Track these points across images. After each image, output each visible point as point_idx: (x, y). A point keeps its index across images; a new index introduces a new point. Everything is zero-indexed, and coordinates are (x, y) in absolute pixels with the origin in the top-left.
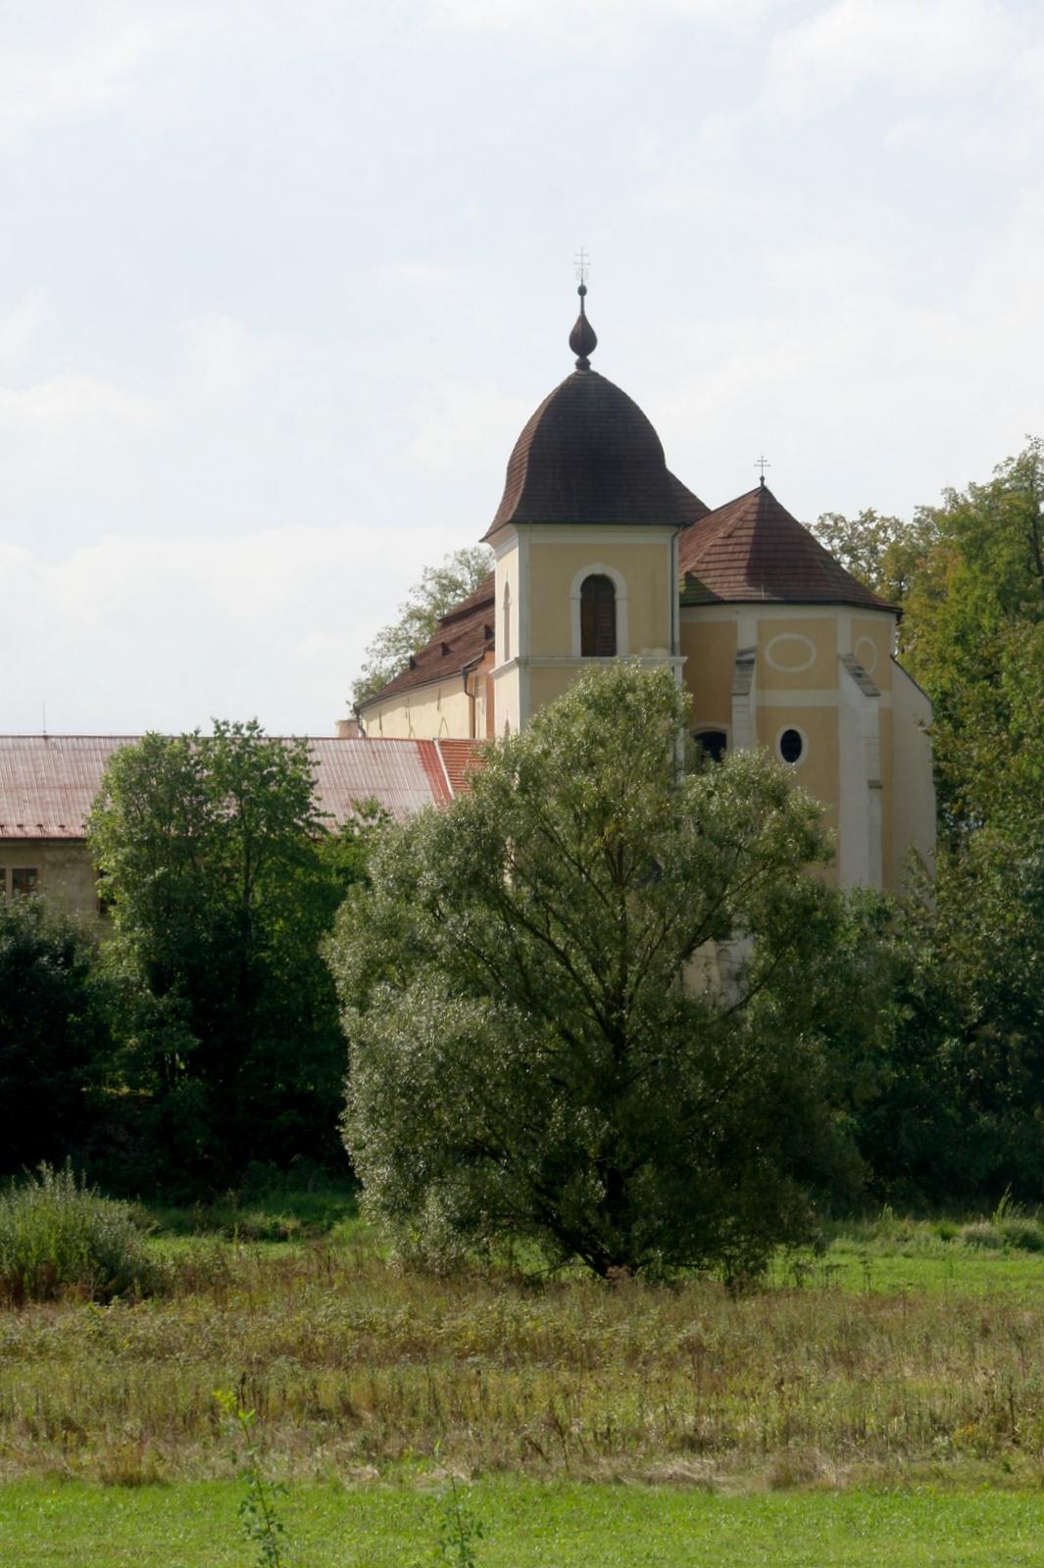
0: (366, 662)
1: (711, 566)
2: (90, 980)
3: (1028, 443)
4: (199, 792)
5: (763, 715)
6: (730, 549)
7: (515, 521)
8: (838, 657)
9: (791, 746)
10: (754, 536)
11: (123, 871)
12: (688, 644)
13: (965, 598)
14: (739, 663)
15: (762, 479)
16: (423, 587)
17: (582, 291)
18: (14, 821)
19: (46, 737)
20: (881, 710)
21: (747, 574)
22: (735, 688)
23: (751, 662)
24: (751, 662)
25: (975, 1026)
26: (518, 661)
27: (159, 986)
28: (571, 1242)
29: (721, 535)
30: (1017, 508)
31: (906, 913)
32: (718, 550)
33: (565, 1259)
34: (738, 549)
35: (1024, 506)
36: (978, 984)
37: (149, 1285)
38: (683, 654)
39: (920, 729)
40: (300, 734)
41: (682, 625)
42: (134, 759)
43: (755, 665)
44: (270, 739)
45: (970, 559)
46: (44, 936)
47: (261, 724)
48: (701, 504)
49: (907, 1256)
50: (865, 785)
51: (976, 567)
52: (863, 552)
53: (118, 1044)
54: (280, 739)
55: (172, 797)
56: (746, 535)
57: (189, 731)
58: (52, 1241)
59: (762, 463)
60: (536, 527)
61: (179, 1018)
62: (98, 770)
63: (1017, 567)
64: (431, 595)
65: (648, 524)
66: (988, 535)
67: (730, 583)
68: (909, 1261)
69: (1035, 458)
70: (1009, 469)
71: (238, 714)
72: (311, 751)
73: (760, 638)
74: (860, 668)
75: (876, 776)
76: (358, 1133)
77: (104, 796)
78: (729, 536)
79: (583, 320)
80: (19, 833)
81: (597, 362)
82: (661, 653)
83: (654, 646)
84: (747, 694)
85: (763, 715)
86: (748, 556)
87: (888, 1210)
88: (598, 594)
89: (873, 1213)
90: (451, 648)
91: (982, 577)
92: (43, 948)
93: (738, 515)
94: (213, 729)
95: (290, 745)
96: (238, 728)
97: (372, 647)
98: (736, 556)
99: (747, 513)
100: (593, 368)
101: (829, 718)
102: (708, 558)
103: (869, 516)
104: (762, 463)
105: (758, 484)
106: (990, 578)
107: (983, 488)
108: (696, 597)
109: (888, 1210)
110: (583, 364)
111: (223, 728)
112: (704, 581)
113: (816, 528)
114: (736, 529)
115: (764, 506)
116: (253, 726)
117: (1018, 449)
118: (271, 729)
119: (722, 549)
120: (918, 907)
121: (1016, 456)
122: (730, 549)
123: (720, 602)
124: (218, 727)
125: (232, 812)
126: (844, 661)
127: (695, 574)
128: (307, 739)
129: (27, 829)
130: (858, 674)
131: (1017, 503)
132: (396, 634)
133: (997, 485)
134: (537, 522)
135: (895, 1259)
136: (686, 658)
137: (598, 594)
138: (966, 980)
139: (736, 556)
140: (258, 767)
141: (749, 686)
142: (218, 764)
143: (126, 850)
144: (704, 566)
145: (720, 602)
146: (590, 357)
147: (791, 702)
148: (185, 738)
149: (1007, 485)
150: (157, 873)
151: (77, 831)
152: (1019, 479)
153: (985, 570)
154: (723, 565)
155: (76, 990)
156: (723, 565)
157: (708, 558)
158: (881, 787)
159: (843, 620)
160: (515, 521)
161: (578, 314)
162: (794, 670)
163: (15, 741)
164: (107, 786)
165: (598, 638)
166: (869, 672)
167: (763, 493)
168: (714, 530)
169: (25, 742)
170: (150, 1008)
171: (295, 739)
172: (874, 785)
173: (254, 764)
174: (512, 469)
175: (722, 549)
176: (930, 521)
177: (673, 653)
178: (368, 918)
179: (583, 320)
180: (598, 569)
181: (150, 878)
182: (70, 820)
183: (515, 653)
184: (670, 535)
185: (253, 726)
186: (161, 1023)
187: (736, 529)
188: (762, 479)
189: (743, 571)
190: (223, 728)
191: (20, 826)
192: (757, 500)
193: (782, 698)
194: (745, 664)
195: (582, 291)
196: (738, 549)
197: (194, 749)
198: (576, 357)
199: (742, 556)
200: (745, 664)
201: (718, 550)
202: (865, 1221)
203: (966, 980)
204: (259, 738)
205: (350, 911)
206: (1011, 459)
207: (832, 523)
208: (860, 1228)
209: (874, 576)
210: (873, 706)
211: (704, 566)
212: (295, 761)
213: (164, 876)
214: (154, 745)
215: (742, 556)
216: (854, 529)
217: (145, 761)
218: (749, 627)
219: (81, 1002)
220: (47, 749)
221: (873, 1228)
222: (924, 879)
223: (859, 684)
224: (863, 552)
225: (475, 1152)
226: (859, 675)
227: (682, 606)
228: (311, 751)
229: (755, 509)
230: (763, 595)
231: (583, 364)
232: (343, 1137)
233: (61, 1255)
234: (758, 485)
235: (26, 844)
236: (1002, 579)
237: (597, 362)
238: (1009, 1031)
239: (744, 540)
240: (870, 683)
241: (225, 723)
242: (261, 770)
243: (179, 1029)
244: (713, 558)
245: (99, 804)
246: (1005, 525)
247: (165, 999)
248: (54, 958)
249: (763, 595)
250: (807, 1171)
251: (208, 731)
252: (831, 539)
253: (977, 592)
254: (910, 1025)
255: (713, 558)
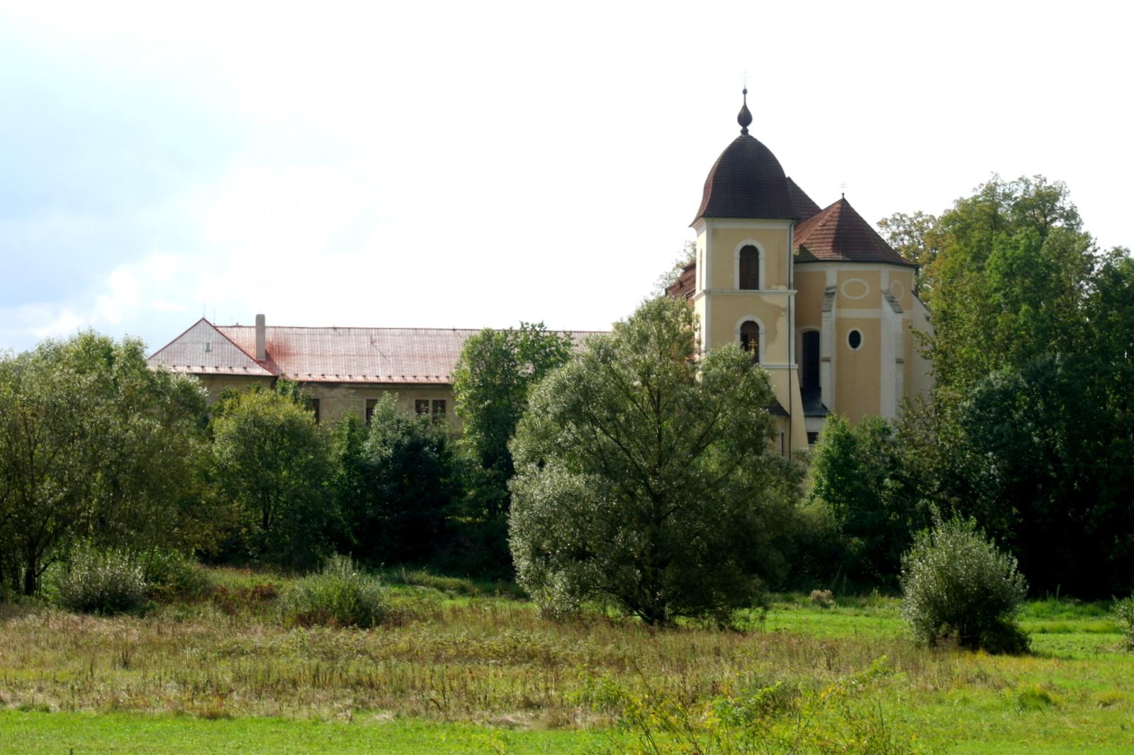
0: (653, 291)
1: (814, 241)
2: (454, 460)
3: (992, 176)
4: (512, 360)
5: (839, 322)
6: (824, 232)
7: (703, 216)
8: (881, 291)
9: (855, 339)
10: (838, 225)
11: (469, 403)
12: (798, 283)
13: (956, 260)
14: (827, 294)
15: (843, 194)
16: (685, 250)
17: (745, 92)
18: (434, 374)
19: (454, 330)
20: (903, 319)
21: (832, 246)
22: (824, 308)
23: (833, 294)
24: (833, 294)
25: (934, 493)
26: (705, 292)
27: (487, 465)
28: (631, 604)
29: (820, 224)
30: (984, 211)
31: (900, 430)
32: (818, 232)
33: (631, 614)
34: (828, 232)
35: (988, 210)
36: (937, 470)
37: (397, 620)
38: (795, 289)
39: (910, 330)
40: (568, 329)
41: (794, 273)
42: (477, 342)
43: (835, 296)
44: (550, 332)
45: (959, 238)
46: (428, 436)
47: (545, 325)
48: (818, 208)
49: (867, 616)
50: (894, 361)
51: (962, 243)
52: (916, 233)
53: (465, 494)
54: (556, 332)
55: (497, 363)
56: (833, 225)
57: (507, 328)
58: (335, 596)
59: (843, 186)
60: (716, 219)
61: (497, 481)
62: (458, 348)
63: (983, 243)
64: (689, 255)
65: (778, 218)
66: (969, 226)
67: (822, 250)
68: (868, 619)
69: (996, 184)
70: (981, 190)
71: (533, 319)
72: (573, 339)
73: (839, 281)
74: (893, 298)
75: (901, 356)
76: (518, 545)
77: (461, 362)
78: (824, 225)
79: (745, 108)
80: (436, 381)
81: (753, 130)
82: (783, 288)
83: (779, 284)
84: (830, 311)
85: (839, 322)
86: (833, 236)
87: (876, 591)
88: (749, 256)
89: (867, 593)
90: (684, 284)
91: (965, 249)
92: (427, 442)
93: (829, 214)
94: (520, 326)
95: (561, 335)
96: (533, 326)
97: (657, 282)
98: (827, 236)
99: (834, 212)
100: (750, 133)
101: (876, 324)
102: (812, 237)
103: (920, 214)
104: (843, 186)
105: (841, 197)
106: (969, 249)
107: (968, 200)
108: (804, 258)
109: (876, 591)
110: (745, 132)
111: (525, 326)
112: (809, 249)
113: (891, 221)
114: (828, 221)
115: (844, 210)
116: (541, 325)
117: (986, 179)
118: (551, 326)
119: (820, 232)
120: (906, 428)
121: (985, 183)
122: (824, 232)
123: (817, 261)
124: (522, 326)
125: (530, 371)
126: (885, 293)
127: (805, 246)
128: (571, 332)
129: (441, 379)
130: (892, 301)
131: (985, 208)
132: (670, 276)
133: (975, 200)
134: (716, 217)
135: (860, 618)
136: (796, 291)
137: (749, 256)
138: (929, 468)
139: (827, 236)
140: (544, 347)
141: (831, 306)
142: (522, 345)
143: (471, 391)
144: (809, 241)
145: (817, 261)
146: (749, 128)
147: (855, 315)
148: (505, 331)
149: (981, 199)
150: (486, 403)
151: (443, 380)
152: (986, 195)
153: (966, 245)
154: (820, 241)
155: (445, 465)
156: (820, 241)
157: (812, 237)
158: (902, 362)
159: (884, 272)
160: (703, 216)
161: (743, 104)
162: (857, 298)
163: (438, 331)
164: (462, 356)
165: (749, 279)
166: (898, 300)
167: (843, 202)
168: (818, 222)
169: (443, 332)
170: (482, 476)
171: (565, 332)
172: (899, 361)
173: (542, 346)
174: (706, 188)
175: (820, 232)
176: (949, 219)
177: (789, 288)
178: (533, 429)
179: (745, 108)
180: (749, 242)
181: (481, 406)
182: (440, 373)
183: (704, 287)
184: (789, 224)
185: (541, 325)
186: (488, 483)
187: (828, 221)
188: (843, 194)
189: (831, 244)
190: (525, 326)
191: (437, 377)
192: (839, 206)
193: (849, 313)
194: (830, 294)
195: (745, 92)
196: (828, 232)
197: (510, 338)
198: (741, 128)
199: (830, 236)
200: (830, 294)
201: (818, 232)
202: (861, 596)
203: (929, 468)
204: (545, 331)
205: (525, 425)
206: (982, 185)
207: (899, 218)
208: (858, 600)
209: (921, 247)
210: (899, 318)
211: (809, 241)
212: (564, 344)
213: (489, 405)
214: (488, 335)
215: (830, 236)
216: (912, 221)
217: (482, 343)
218: (832, 275)
219: (447, 472)
220: (455, 336)
221: (864, 601)
222: (910, 412)
223: (892, 306)
224: (916, 233)
225: (581, 554)
226: (892, 301)
227: (795, 263)
228: (573, 339)
229: (839, 210)
230: (840, 257)
231: (745, 132)
232: (510, 545)
233: (340, 604)
234: (841, 197)
235: (409, 387)
236: (975, 250)
237: (753, 130)
238: (953, 495)
239: (832, 227)
240: (899, 306)
241: (527, 324)
242: (545, 348)
243: (497, 486)
244: (815, 237)
245: (459, 365)
246: (977, 221)
247: (489, 470)
248: (432, 448)
249: (840, 257)
250: (754, 567)
251: (517, 327)
252: (898, 226)
253: (962, 257)
254: (899, 491)
255: (815, 237)
